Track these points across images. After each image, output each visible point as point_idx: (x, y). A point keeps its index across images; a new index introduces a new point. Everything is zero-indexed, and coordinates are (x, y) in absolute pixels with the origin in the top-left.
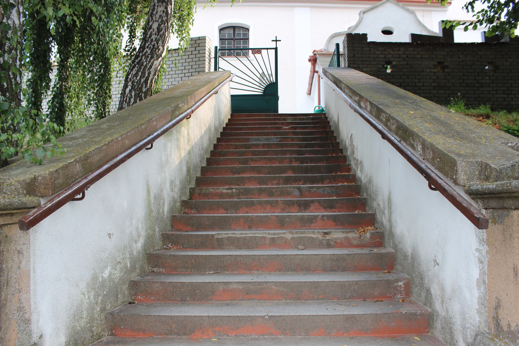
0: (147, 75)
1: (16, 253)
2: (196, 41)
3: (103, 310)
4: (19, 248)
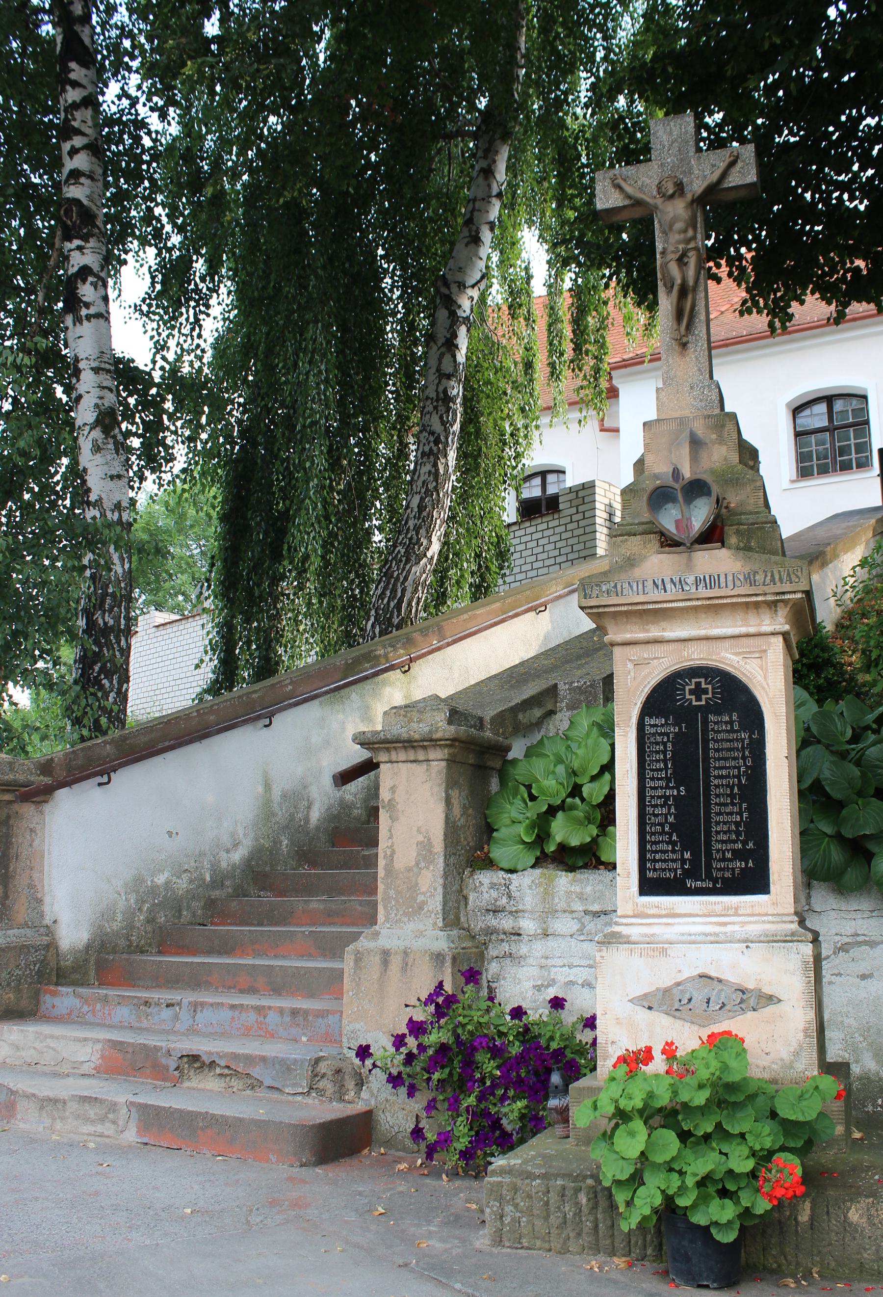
0: (399, 594)
1: (28, 832)
2: (577, 492)
3: (150, 921)
4: (31, 826)
